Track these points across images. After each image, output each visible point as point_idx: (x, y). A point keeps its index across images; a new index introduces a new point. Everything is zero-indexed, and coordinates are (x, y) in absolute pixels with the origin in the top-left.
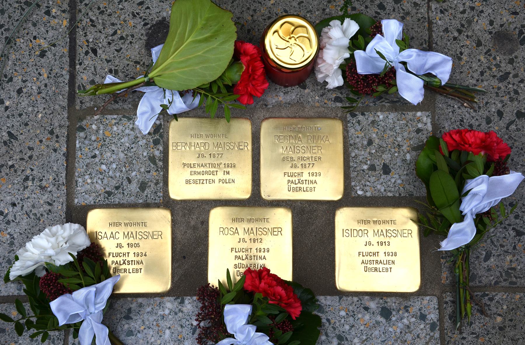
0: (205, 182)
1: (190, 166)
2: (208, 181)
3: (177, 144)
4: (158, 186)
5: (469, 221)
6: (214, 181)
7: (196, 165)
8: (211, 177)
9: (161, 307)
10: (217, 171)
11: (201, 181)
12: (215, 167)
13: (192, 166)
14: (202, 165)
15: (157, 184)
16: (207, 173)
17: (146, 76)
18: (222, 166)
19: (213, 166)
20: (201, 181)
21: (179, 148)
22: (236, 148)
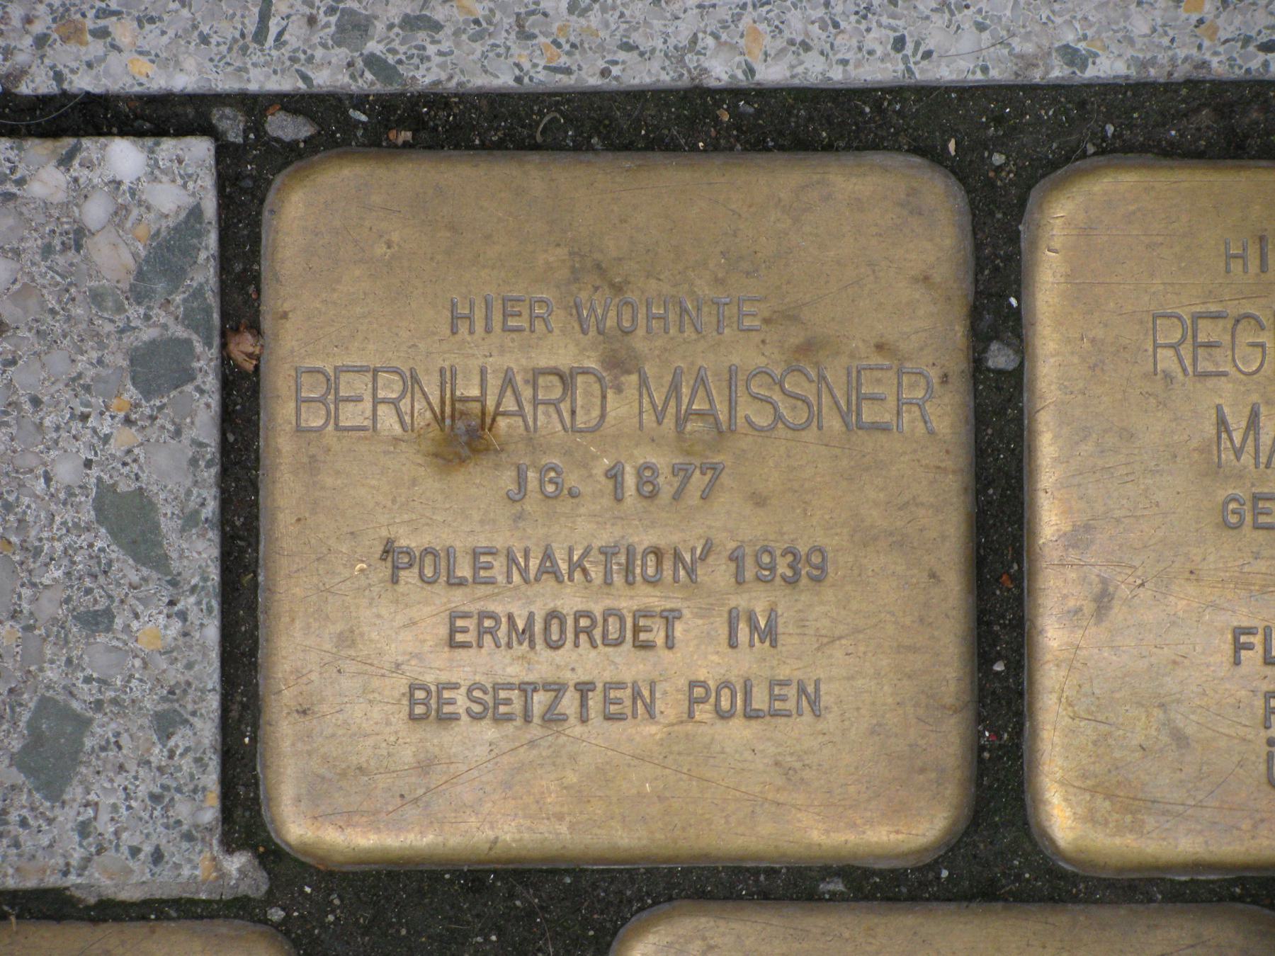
0: (569, 703)
1: (437, 566)
2: (595, 701)
3: (332, 383)
4: (179, 740)
5: (185, 335)
6: (643, 700)
7: (499, 564)
8: (626, 665)
9: (191, 719)
10: (670, 618)
11: (540, 700)
12: (651, 582)
13: (464, 571)
14: (548, 568)
15: (166, 724)
16: (586, 629)
17: (188, 342)
18: (718, 574)
19: (625, 564)
20: (540, 700)
21: (352, 415)
22: (834, 423)
